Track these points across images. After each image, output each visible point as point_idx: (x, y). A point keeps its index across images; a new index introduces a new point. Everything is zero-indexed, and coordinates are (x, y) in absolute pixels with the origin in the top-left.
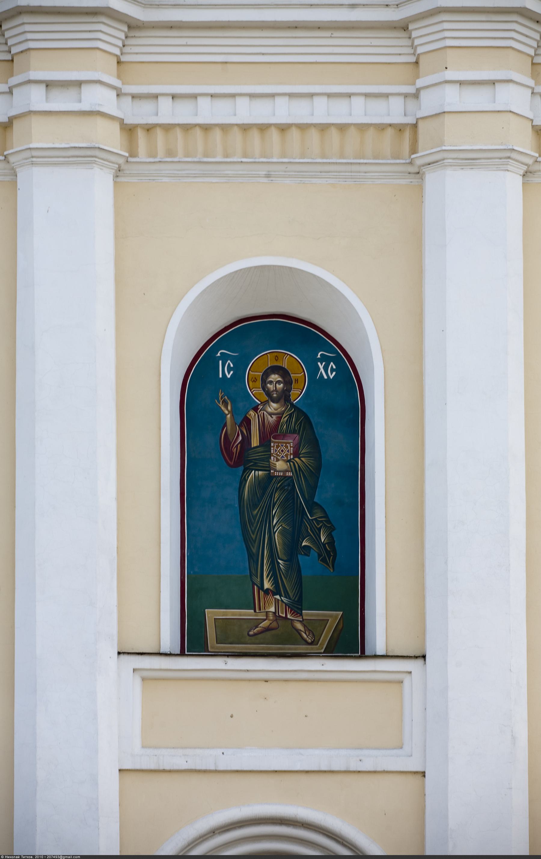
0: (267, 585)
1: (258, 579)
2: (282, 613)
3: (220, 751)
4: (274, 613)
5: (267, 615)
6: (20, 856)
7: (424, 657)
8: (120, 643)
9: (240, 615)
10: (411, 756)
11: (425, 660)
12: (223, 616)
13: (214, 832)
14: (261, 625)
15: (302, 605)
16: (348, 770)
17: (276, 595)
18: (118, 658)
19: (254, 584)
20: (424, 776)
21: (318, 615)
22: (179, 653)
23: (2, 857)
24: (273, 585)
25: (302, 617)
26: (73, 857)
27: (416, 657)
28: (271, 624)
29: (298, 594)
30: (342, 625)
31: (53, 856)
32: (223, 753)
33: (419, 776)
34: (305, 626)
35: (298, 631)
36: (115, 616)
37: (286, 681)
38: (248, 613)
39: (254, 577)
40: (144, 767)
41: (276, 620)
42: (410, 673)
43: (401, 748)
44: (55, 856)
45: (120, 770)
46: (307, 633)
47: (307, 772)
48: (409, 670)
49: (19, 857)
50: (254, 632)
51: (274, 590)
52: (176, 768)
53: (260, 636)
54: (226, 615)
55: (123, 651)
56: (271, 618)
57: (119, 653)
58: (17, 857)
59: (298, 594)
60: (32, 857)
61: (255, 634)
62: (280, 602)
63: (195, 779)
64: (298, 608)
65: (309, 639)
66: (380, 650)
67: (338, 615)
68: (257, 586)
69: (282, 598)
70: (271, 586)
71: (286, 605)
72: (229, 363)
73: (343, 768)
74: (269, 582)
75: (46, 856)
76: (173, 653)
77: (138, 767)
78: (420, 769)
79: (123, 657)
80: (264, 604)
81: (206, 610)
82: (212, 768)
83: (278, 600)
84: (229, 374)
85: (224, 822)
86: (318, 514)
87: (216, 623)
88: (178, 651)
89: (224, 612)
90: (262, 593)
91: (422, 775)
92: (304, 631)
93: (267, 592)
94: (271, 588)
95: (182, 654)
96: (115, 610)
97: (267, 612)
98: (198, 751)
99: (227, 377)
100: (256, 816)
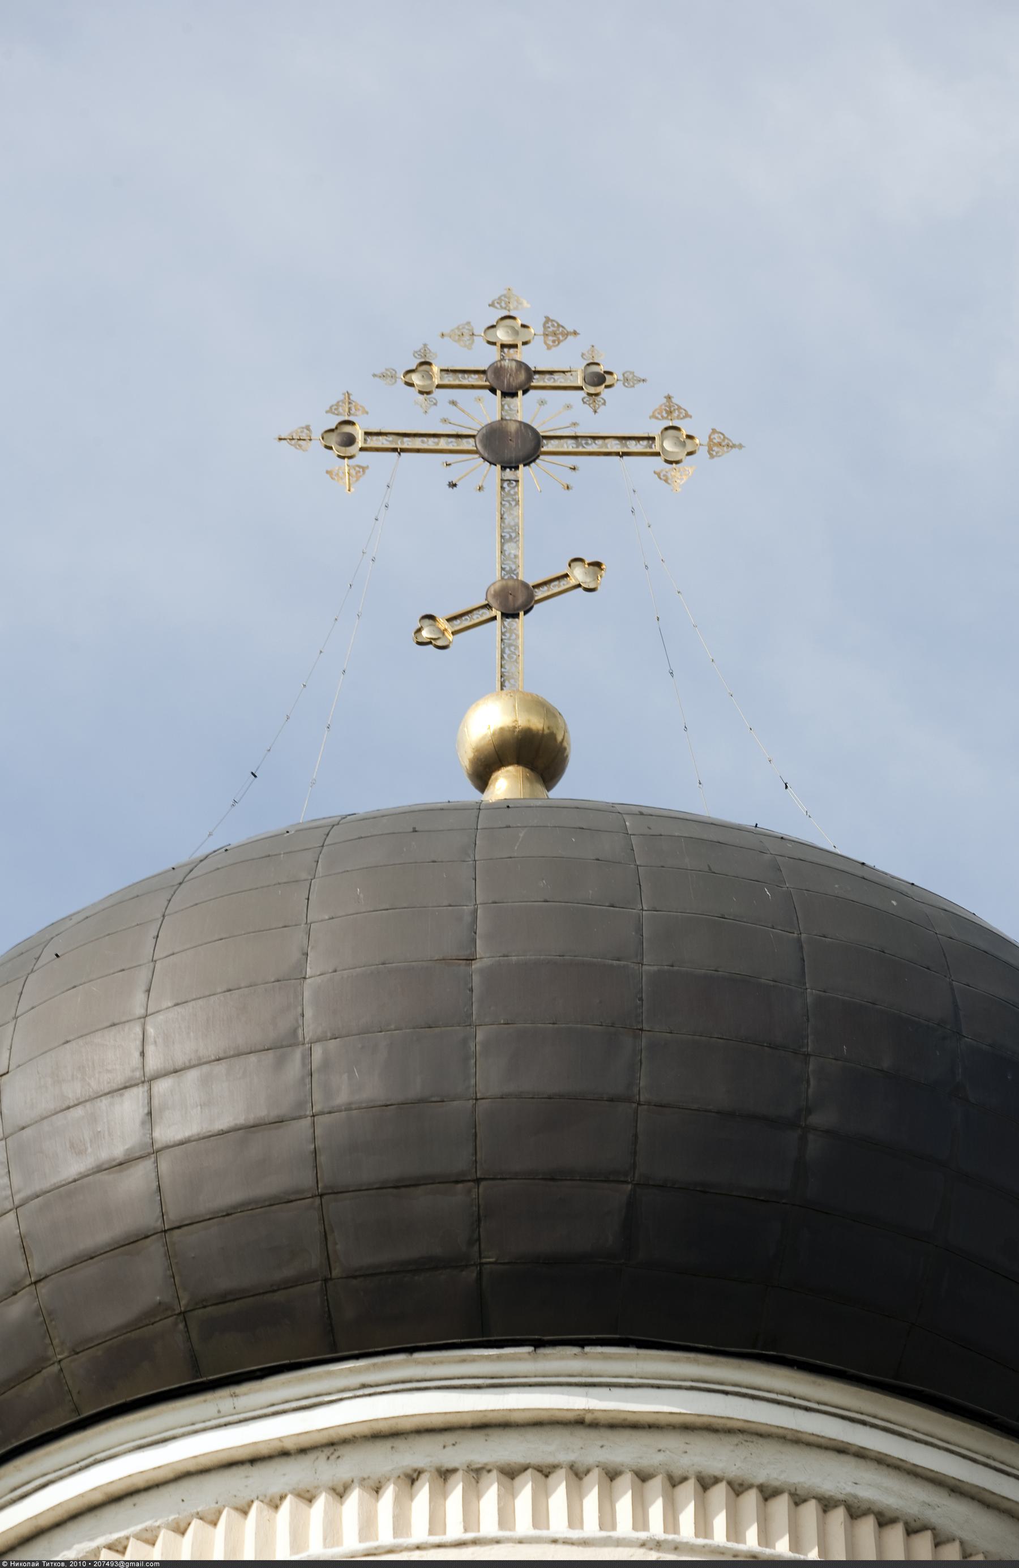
6: (40, 1562)
26: (145, 1564)
31: (107, 1561)
44: (110, 1561)
49: (37, 1564)
58: (33, 1565)
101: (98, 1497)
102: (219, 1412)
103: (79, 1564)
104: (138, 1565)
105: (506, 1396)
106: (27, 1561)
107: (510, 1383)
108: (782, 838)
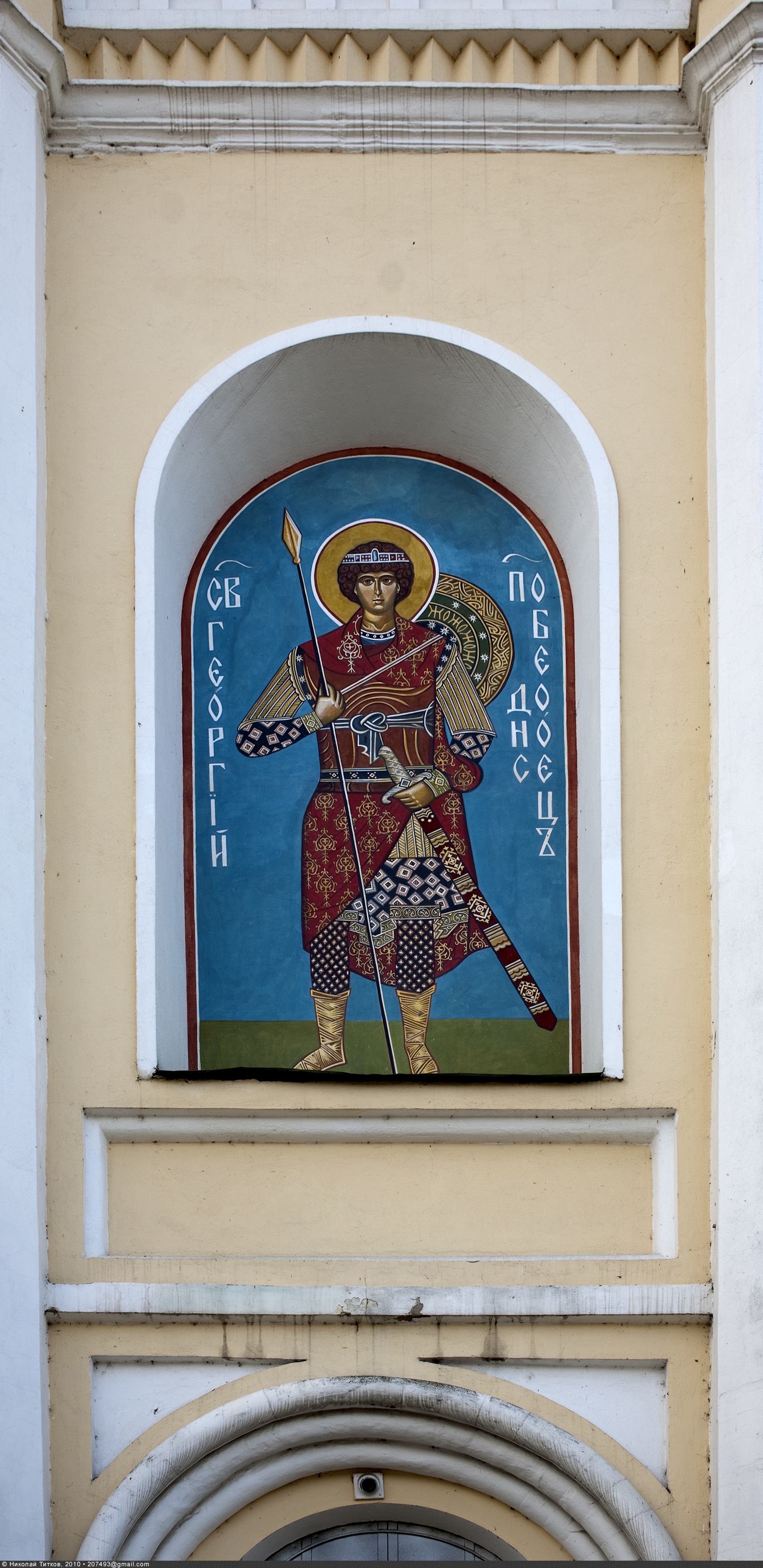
6: (38, 1562)
23: (4, 1565)
26: (135, 1564)
31: (100, 1562)
44: (103, 1562)
49: (35, 1565)
58: (31, 1565)
72: (544, 758)
75: (86, 1562)
84: (217, 681)
86: (402, 685)
99: (213, 719)
100: (339, 102)
101: (597, 1541)
102: (369, 1487)
103: (73, 1564)
104: (129, 1565)
105: (277, 1367)
106: (25, 1562)
107: (424, 1468)
108: (621, 698)
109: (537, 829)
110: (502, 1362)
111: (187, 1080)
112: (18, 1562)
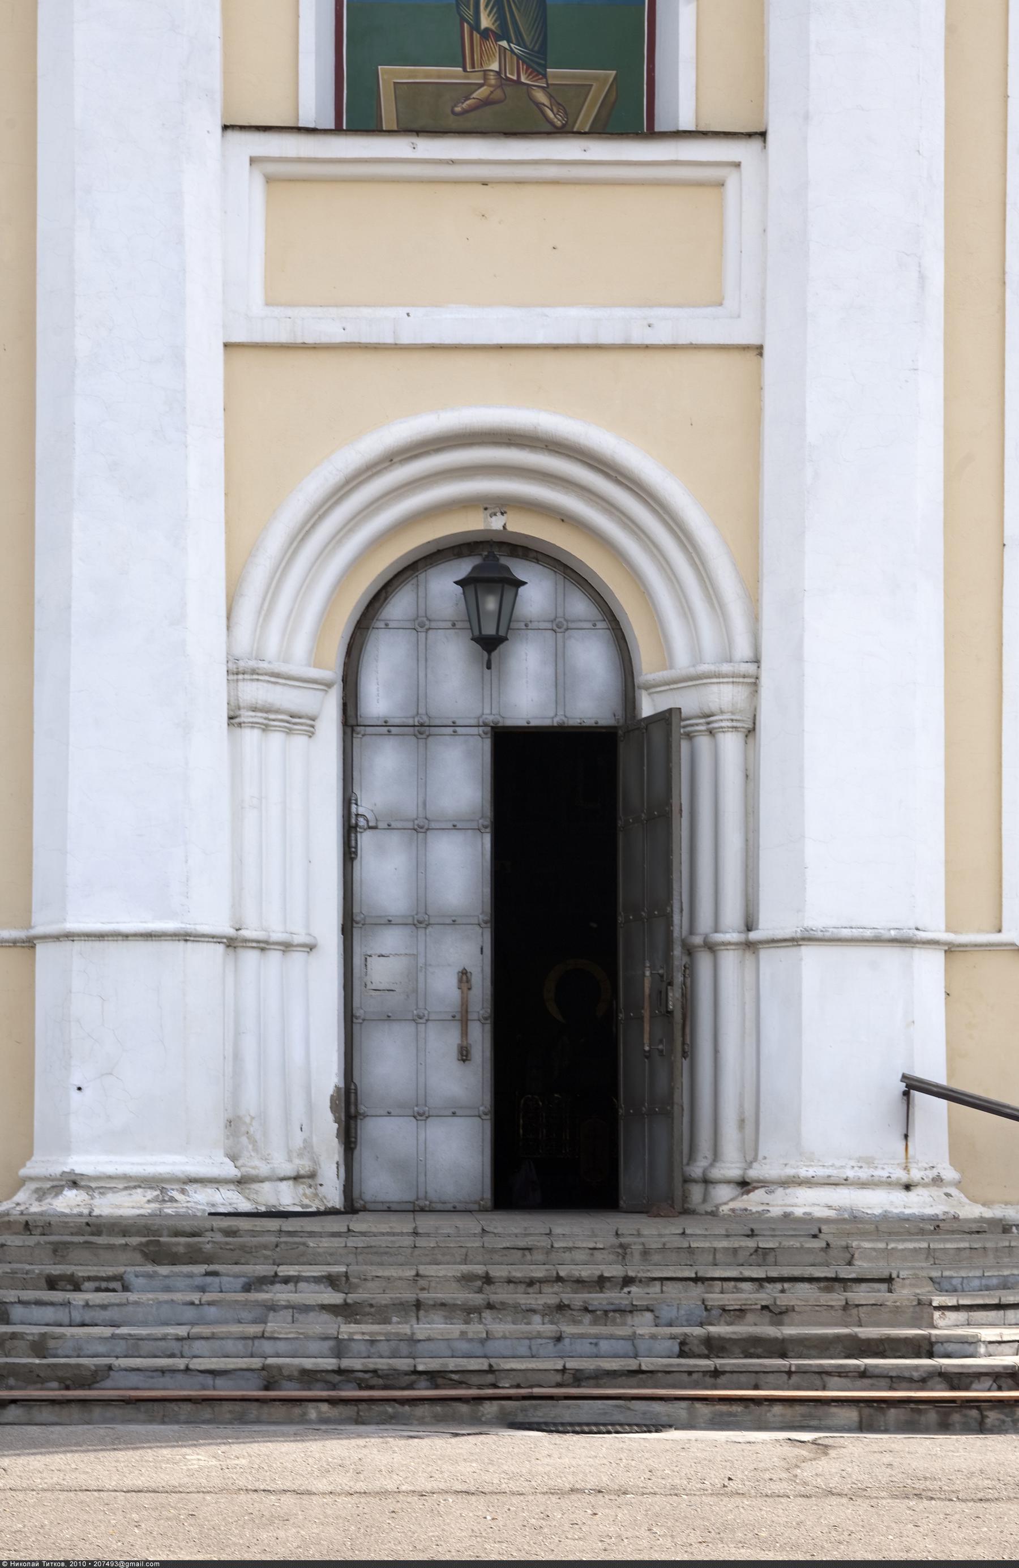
0: (485, 22)
1: (469, 9)
2: (512, 74)
3: (402, 312)
4: (498, 73)
5: (485, 77)
6: (40, 1562)
7: (763, 135)
8: (226, 110)
9: (439, 77)
10: (739, 316)
11: (765, 141)
12: (409, 78)
13: (391, 460)
14: (474, 95)
15: (546, 60)
16: (628, 343)
17: (502, 39)
18: (223, 136)
19: (463, 20)
20: (761, 354)
21: (574, 77)
22: (333, 127)
24: (495, 21)
25: (547, 81)
26: (145, 1564)
27: (750, 135)
28: (492, 92)
29: (539, 42)
30: (614, 93)
31: (107, 1561)
32: (408, 315)
33: (751, 355)
34: (550, 97)
35: (538, 105)
36: (217, 56)
37: (520, 182)
38: (451, 75)
39: (463, 8)
40: (269, 339)
41: (501, 86)
42: (738, 165)
43: (721, 304)
45: (226, 345)
46: (555, 110)
47: (556, 348)
48: (737, 160)
49: (37, 1564)
50: (463, 108)
51: (499, 32)
52: (325, 340)
53: (472, 114)
54: (415, 77)
55: (232, 124)
56: (493, 82)
57: (225, 128)
58: (33, 1565)
59: (539, 42)
60: (63, 1564)
61: (465, 112)
62: (508, 53)
63: (359, 361)
64: (539, 64)
65: (559, 120)
66: (686, 121)
67: (607, 77)
68: (469, 23)
69: (512, 45)
70: (493, 24)
71: (518, 57)
73: (619, 341)
74: (489, 15)
75: (92, 1562)
76: (319, 127)
77: (257, 338)
78: (754, 341)
79: (234, 136)
80: (481, 57)
81: (379, 67)
82: (389, 340)
83: (505, 48)
85: (409, 440)
87: (397, 92)
88: (331, 125)
89: (410, 71)
90: (476, 36)
91: (756, 352)
92: (549, 106)
93: (485, 34)
94: (493, 28)
95: (338, 130)
96: (217, 44)
97: (485, 71)
98: (366, 312)
104: (138, 1565)
106: (27, 1561)
109: (614, 72)
110: (485, 666)
111: (806, 1216)
112: (20, 1561)
